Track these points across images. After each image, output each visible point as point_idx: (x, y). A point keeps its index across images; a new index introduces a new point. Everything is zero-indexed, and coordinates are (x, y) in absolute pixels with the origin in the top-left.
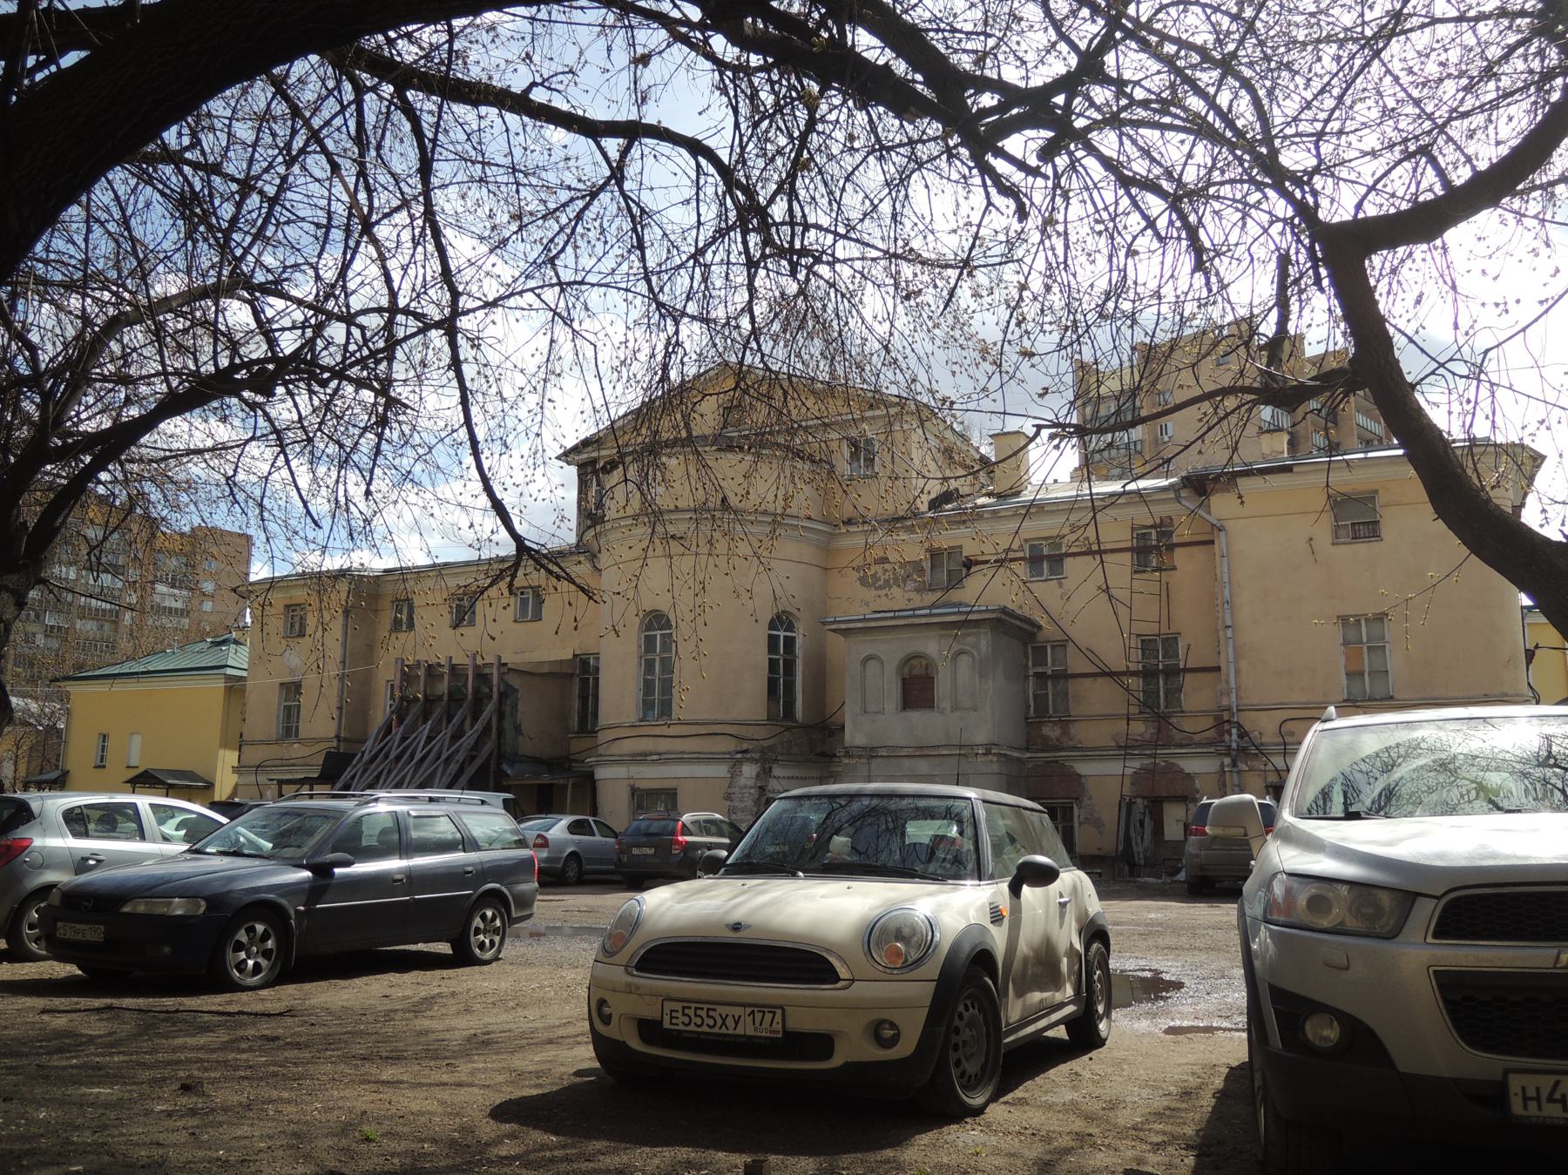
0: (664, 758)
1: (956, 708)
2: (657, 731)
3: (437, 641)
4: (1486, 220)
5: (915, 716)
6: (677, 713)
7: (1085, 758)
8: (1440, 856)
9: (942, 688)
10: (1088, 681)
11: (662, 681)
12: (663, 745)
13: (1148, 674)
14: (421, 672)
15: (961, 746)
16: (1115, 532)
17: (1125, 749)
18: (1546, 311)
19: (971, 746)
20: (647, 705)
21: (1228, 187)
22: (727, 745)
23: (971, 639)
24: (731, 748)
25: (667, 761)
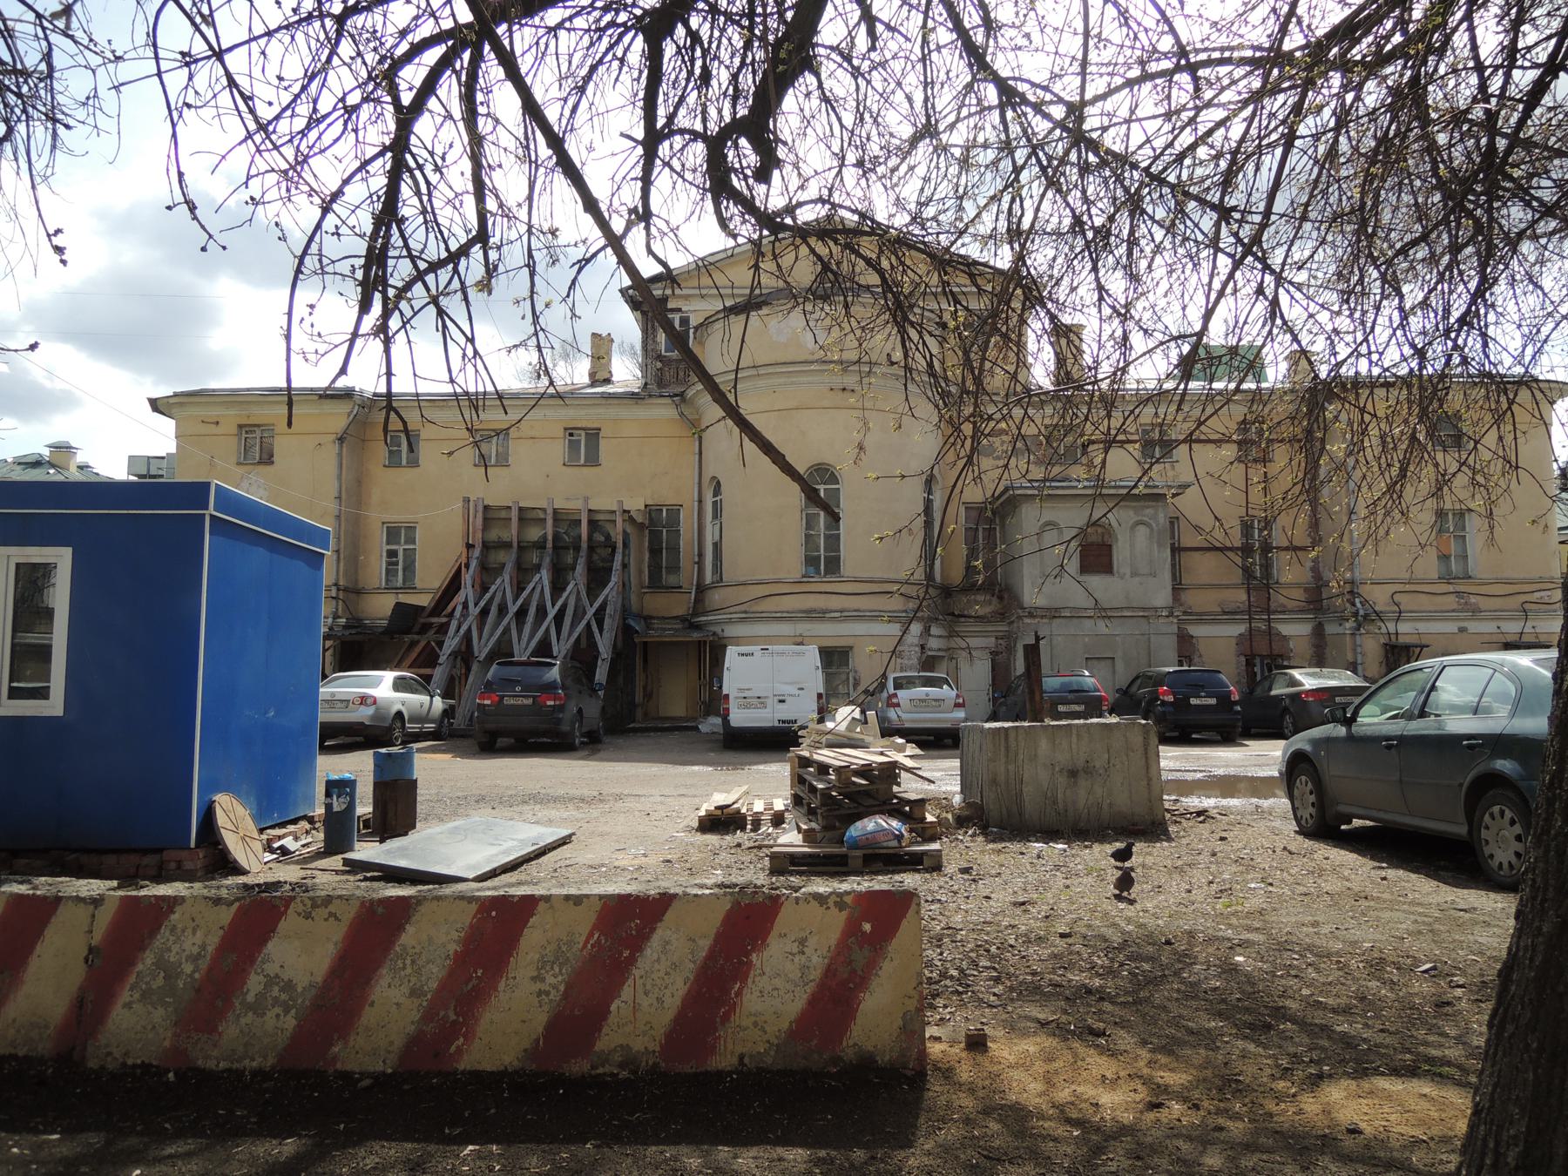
0: (846, 616)
1: (1134, 574)
2: (828, 588)
3: (538, 478)
4: (527, 192)
5: (1096, 581)
6: (848, 567)
7: (1201, 621)
8: (736, 766)
9: (1121, 554)
10: (1197, 555)
11: (827, 537)
12: (835, 602)
13: (1246, 550)
14: (514, 514)
15: (1144, 609)
16: (1225, 422)
17: (1228, 614)
18: (290, 314)
19: (1156, 609)
20: (812, 561)
21: (1516, 73)
22: (896, 604)
23: (1148, 511)
24: (901, 607)
25: (847, 619)
